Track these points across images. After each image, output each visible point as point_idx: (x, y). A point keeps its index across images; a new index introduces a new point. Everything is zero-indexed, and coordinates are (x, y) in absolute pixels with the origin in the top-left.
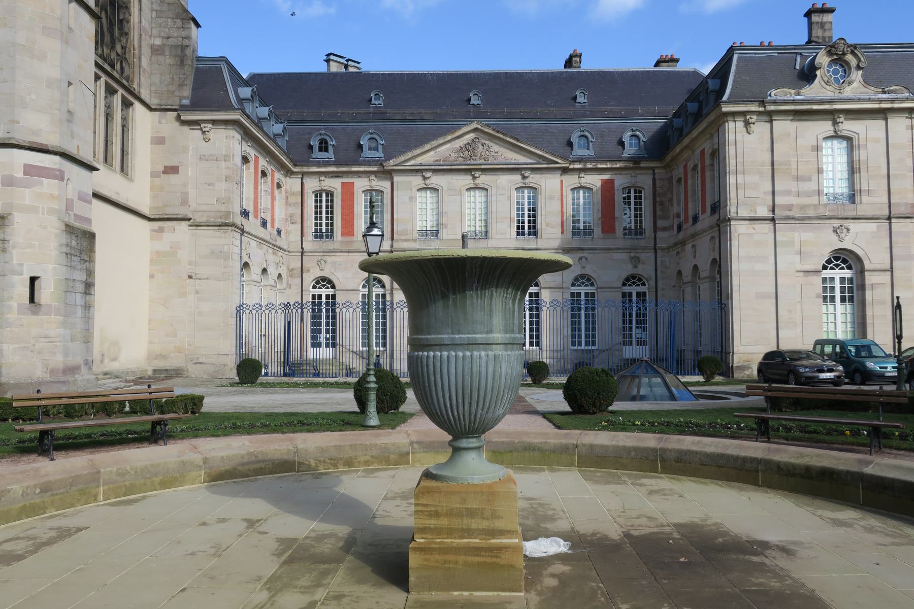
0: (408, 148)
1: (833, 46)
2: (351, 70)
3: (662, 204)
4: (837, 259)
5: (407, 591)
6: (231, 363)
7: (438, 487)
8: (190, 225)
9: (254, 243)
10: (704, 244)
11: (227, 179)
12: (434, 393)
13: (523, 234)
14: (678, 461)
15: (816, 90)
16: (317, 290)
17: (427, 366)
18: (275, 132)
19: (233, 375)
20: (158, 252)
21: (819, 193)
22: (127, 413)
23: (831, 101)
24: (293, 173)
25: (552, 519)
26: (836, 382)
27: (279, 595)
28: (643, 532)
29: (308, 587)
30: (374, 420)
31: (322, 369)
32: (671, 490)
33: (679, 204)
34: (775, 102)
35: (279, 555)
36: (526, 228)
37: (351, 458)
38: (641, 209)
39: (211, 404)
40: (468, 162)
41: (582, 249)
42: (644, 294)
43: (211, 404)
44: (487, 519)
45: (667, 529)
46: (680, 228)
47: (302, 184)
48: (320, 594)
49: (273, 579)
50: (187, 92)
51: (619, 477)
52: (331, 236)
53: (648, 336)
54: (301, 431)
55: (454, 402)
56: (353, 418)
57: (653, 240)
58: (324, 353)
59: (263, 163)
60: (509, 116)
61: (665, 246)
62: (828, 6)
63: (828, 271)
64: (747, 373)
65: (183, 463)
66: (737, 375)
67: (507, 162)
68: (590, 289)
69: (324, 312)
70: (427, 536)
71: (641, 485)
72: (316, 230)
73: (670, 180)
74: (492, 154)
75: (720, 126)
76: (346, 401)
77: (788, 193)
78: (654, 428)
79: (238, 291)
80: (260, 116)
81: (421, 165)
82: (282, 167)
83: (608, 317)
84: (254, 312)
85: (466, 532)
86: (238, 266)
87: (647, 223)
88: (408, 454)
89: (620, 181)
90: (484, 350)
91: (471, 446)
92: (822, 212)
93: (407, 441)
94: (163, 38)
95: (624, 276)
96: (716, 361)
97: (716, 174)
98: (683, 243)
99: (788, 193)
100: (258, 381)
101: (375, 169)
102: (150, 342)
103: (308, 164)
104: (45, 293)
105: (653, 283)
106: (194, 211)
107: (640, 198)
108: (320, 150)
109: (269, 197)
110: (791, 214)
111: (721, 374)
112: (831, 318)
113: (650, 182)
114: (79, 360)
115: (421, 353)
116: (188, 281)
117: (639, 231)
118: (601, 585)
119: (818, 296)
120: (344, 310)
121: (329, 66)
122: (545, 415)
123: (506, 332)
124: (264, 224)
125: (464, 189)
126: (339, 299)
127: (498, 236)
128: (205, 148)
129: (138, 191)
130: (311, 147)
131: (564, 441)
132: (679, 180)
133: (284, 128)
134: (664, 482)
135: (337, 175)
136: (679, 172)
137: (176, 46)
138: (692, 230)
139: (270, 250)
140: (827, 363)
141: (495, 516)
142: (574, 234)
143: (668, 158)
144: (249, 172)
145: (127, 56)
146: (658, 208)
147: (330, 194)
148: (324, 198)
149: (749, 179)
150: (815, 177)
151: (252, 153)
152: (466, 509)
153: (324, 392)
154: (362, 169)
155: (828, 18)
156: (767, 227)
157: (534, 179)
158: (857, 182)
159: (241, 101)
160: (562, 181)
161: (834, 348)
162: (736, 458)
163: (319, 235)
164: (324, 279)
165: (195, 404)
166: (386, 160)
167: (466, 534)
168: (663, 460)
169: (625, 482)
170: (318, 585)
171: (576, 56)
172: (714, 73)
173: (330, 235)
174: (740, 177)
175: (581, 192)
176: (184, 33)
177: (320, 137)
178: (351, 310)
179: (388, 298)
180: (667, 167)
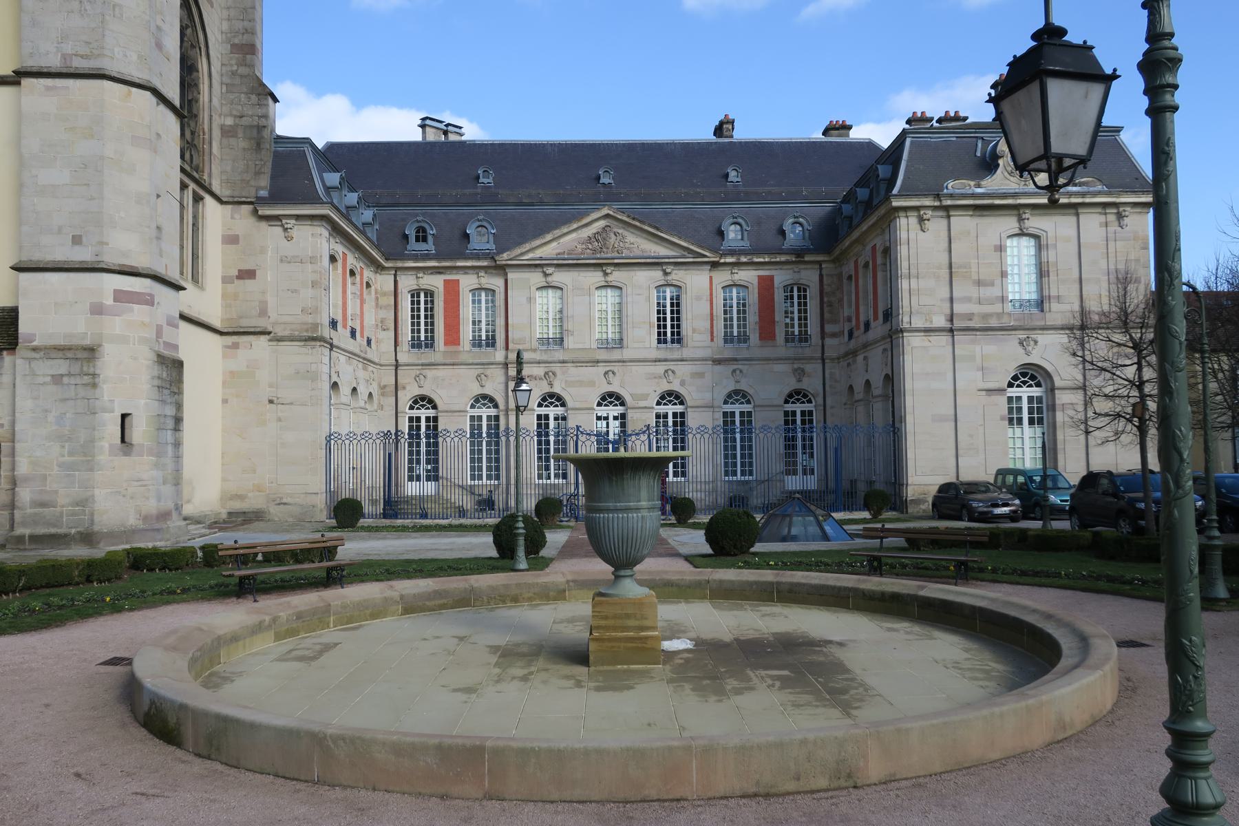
2: (452, 138)
3: (830, 305)
4: (1024, 375)
8: (270, 340)
9: (343, 359)
10: (876, 354)
11: (314, 284)
13: (665, 342)
14: (790, 591)
18: (348, 204)
20: (232, 373)
21: (1003, 299)
22: (260, 562)
23: (1015, 195)
24: (384, 268)
26: (1012, 517)
30: (523, 565)
31: (430, 507)
33: (850, 306)
34: (951, 196)
36: (669, 334)
41: (735, 360)
42: (810, 413)
47: (396, 282)
50: (265, 181)
52: (432, 346)
57: (820, 349)
59: (352, 260)
60: (646, 199)
61: (835, 355)
63: (1015, 389)
65: (386, 599)
66: (912, 510)
68: (746, 408)
69: (424, 438)
72: (413, 338)
73: (840, 276)
76: (484, 545)
77: (968, 300)
81: (541, 259)
86: (327, 386)
87: (813, 328)
89: (781, 277)
92: (1006, 322)
93: (563, 580)
94: (235, 116)
95: (787, 392)
96: (886, 494)
98: (854, 353)
99: (968, 300)
101: (485, 263)
102: (224, 480)
104: (140, 431)
105: (820, 401)
106: (275, 323)
107: (805, 297)
108: (417, 240)
109: (358, 301)
111: (893, 509)
112: (1019, 444)
114: (170, 505)
116: (269, 406)
117: (804, 338)
119: (1002, 419)
121: (424, 132)
122: (688, 558)
124: (353, 333)
125: (593, 288)
126: (572, 423)
127: (636, 345)
128: (288, 248)
129: (208, 300)
130: (406, 237)
132: (850, 278)
134: (778, 609)
136: (849, 268)
137: (251, 127)
139: (360, 365)
140: (1002, 496)
141: (643, 618)
142: (726, 341)
143: (837, 252)
144: (336, 274)
145: (196, 142)
146: (826, 309)
149: (923, 283)
150: (998, 282)
151: (339, 249)
153: (438, 536)
154: (469, 263)
156: (944, 339)
157: (677, 275)
158: (1046, 286)
159: (328, 189)
161: (1015, 479)
162: (834, 588)
163: (416, 344)
164: (423, 398)
168: (778, 592)
171: (728, 123)
173: (430, 343)
174: (913, 281)
175: (734, 290)
176: (260, 112)
177: (417, 225)
180: (837, 261)
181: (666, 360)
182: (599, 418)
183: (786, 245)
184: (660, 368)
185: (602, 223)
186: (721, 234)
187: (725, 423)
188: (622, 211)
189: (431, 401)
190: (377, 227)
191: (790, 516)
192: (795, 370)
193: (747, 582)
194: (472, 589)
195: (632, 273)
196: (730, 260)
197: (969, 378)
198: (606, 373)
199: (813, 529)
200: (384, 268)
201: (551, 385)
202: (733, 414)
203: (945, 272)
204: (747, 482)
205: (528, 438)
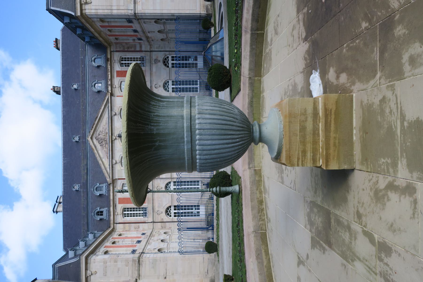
0: (101, 172)
2: (61, 201)
3: (128, 48)
5: (353, 170)
6: (207, 256)
7: (286, 151)
8: (139, 279)
9: (149, 247)
11: (116, 261)
12: (224, 155)
14: (257, 21)
16: (172, 215)
17: (206, 159)
19: (213, 255)
24: (114, 228)
25: (295, 86)
27: (358, 255)
28: (304, 30)
29: (351, 235)
30: (236, 188)
32: (274, 23)
35: (324, 249)
37: (258, 201)
38: (131, 58)
39: (228, 271)
40: (108, 142)
43: (228, 271)
44: (306, 118)
45: (301, 17)
46: (140, 39)
47: (119, 223)
48: (356, 227)
49: (344, 256)
51: (267, 53)
52: (146, 208)
53: (193, 55)
54: (242, 226)
55: (230, 141)
56: (235, 198)
57: (146, 53)
58: (202, 211)
59: (108, 243)
60: (85, 123)
61: (149, 46)
64: (209, 7)
67: (108, 123)
70: (318, 158)
71: (272, 40)
72: (142, 216)
73: (116, 43)
74: (104, 130)
75: (88, 17)
76: (226, 203)
78: (239, 42)
79: (172, 254)
80: (84, 246)
81: (109, 165)
82: (110, 233)
83: (185, 75)
84: (182, 246)
85: (315, 132)
86: (160, 255)
88: (255, 170)
89: (117, 68)
90: (195, 121)
91: (258, 130)
93: (248, 171)
97: (112, 20)
98: (147, 38)
100: (216, 243)
101: (111, 188)
103: (109, 221)
105: (167, 53)
106: (132, 277)
107: (125, 58)
108: (102, 215)
109: (126, 240)
111: (210, 19)
113: (118, 53)
115: (198, 164)
116: (167, 278)
118: (345, 45)
120: (181, 202)
121: (59, 212)
123: (183, 106)
124: (139, 242)
126: (176, 204)
130: (101, 219)
131: (247, 85)
133: (91, 233)
134: (270, 29)
135: (115, 206)
136: (112, 39)
139: (152, 238)
141: (304, 113)
143: (106, 44)
146: (130, 50)
147: (124, 210)
148: (126, 212)
151: (102, 249)
152: (300, 132)
159: (76, 256)
160: (117, 96)
163: (145, 215)
164: (166, 211)
165: (228, 279)
166: (107, 183)
167: (317, 132)
168: (257, 30)
169: (270, 50)
170: (349, 228)
172: (62, 20)
174: (114, 8)
178: (181, 198)
179: (175, 180)
180: (110, 44)
183: (104, 65)
185: (95, 140)
186: (99, 92)
188: (89, 132)
189: (168, 209)
190: (96, 232)
191: (212, 56)
192: (155, 63)
193: (251, 51)
194: (255, 232)
195: (115, 128)
196: (110, 88)
199: (218, 45)
200: (114, 228)
204: (200, 82)
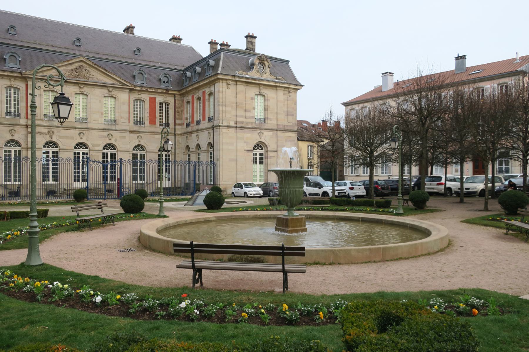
1: (260, 57)
3: (178, 112)
4: (258, 145)
15: (253, 74)
23: (259, 80)
34: (239, 77)
41: (139, 132)
42: (169, 156)
46: (188, 125)
61: (180, 133)
62: (255, 35)
67: (100, 81)
73: (183, 101)
74: (91, 76)
77: (242, 116)
89: (159, 99)
98: (191, 133)
99: (242, 116)
110: (243, 126)
113: (173, 101)
117: (167, 125)
126: (118, 158)
127: (94, 122)
138: (196, 127)
146: (177, 114)
155: (253, 40)
181: (108, 130)
182: (44, 153)
184: (106, 133)
185: (79, 64)
187: (133, 158)
195: (93, 89)
196: (138, 89)
197: (242, 146)
198: (80, 134)
201: (51, 137)
202: (137, 155)
203: (235, 105)
205: (125, 164)
